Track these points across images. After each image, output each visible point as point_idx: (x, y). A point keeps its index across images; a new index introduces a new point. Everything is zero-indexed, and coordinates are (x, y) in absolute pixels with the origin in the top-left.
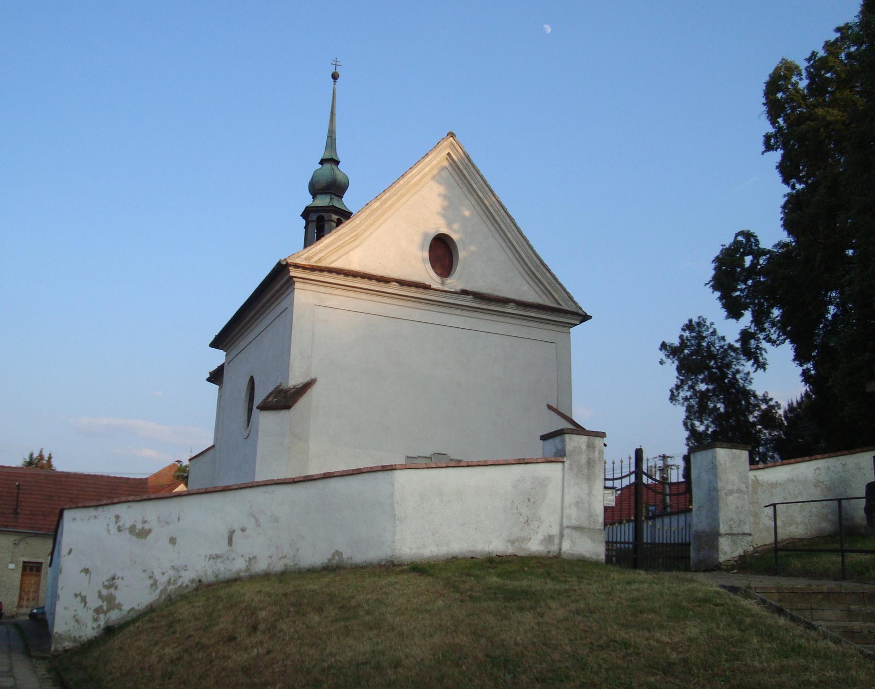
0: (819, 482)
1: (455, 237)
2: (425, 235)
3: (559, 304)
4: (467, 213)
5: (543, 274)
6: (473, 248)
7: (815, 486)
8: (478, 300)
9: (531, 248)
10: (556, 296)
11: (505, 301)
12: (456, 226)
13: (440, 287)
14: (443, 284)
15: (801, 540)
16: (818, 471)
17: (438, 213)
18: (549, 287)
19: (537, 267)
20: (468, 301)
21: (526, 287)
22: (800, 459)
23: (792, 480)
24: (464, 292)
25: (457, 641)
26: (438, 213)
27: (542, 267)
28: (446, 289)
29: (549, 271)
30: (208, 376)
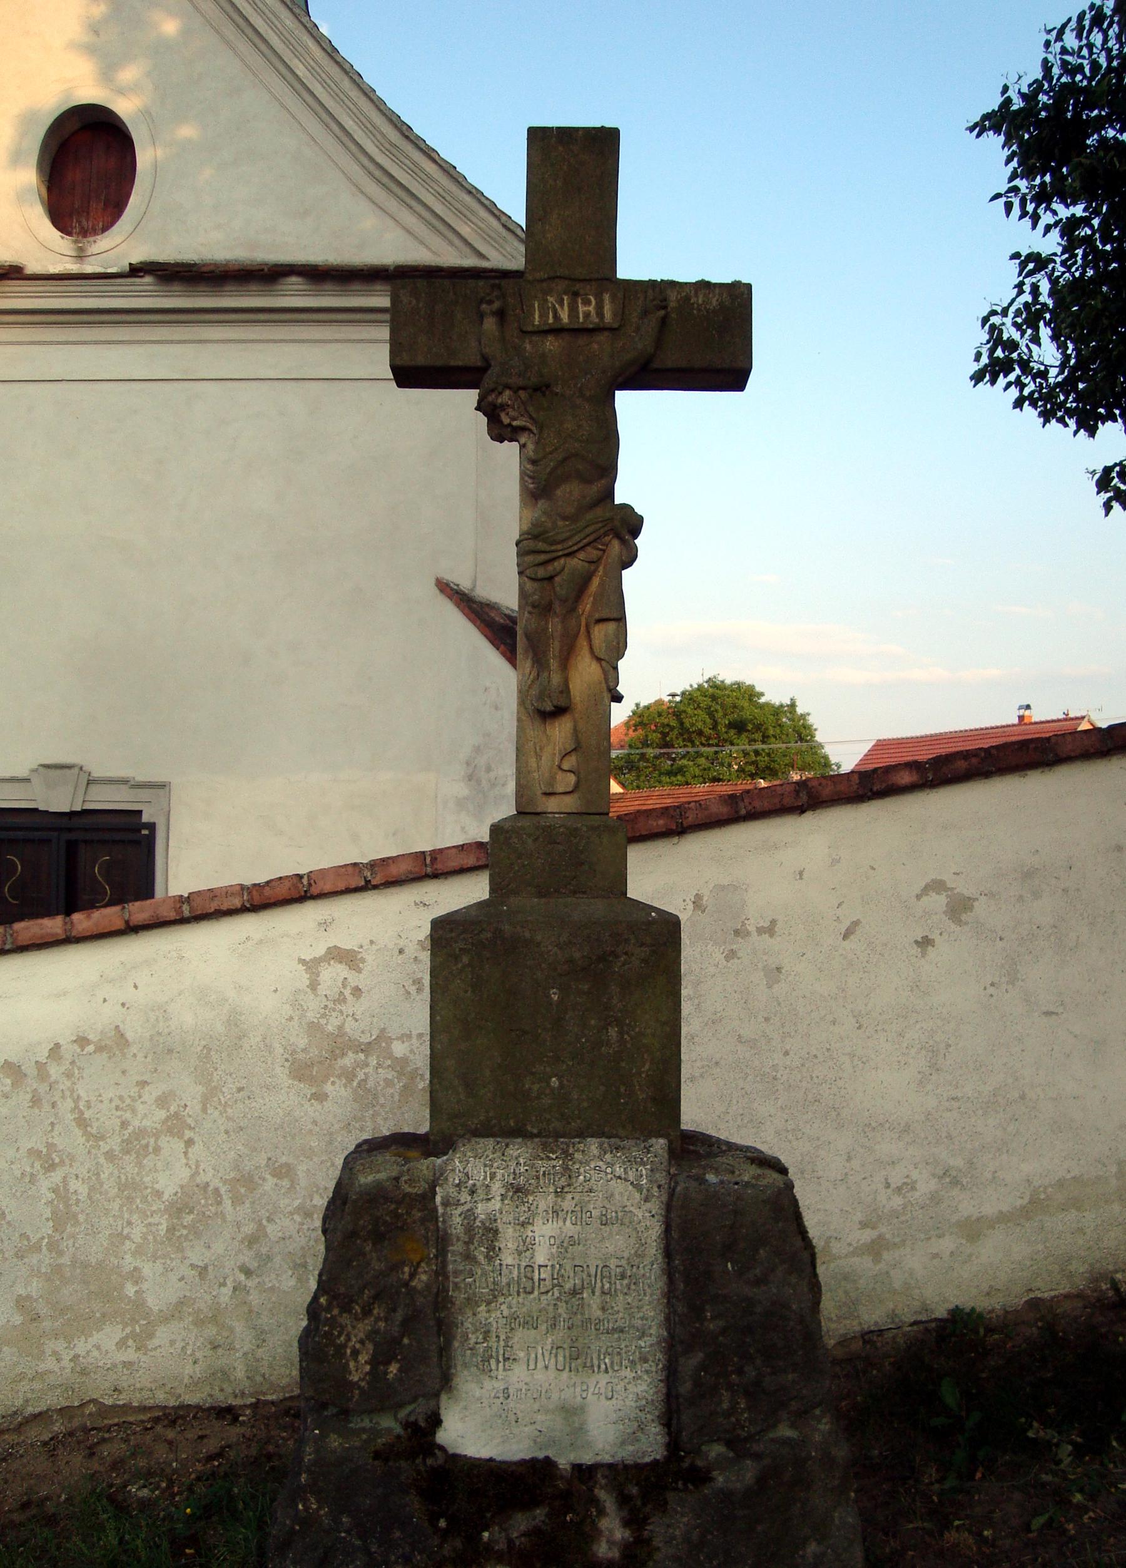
0: (339, 1044)
1: (124, 108)
2: (27, 119)
3: (481, 256)
4: (170, 27)
5: (415, 170)
6: (187, 132)
7: (301, 1071)
8: (177, 287)
9: (368, 93)
10: (465, 230)
11: (270, 275)
12: (129, 74)
13: (73, 267)
14: (80, 256)
15: (175, 1417)
16: (333, 975)
17: (72, 46)
18: (439, 209)
19: (391, 150)
20: (146, 295)
21: (369, 221)
22: (54, 925)
23: (115, 1043)
24: (136, 271)
25: (400, 1318)
26: (72, 46)
27: (409, 148)
28: (89, 269)
29: (429, 153)
30: (1096, 489)
